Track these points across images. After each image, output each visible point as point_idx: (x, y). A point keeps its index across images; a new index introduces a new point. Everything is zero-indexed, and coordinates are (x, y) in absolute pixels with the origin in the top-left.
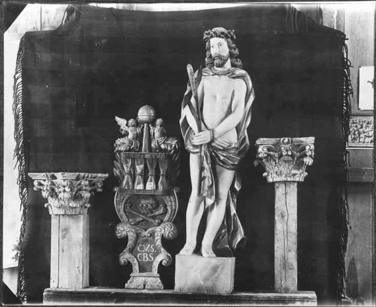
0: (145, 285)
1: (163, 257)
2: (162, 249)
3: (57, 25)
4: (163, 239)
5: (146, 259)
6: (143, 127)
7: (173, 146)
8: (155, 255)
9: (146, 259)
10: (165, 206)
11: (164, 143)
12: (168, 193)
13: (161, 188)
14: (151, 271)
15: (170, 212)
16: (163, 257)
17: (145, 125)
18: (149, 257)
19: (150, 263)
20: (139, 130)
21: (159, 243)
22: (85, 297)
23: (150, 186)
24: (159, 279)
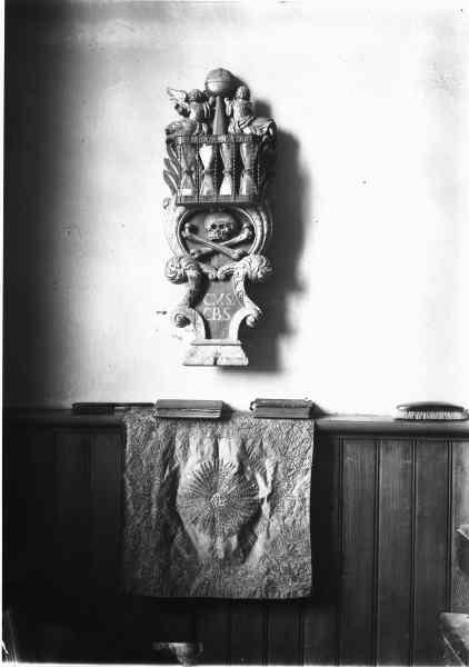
0: (216, 360)
1: (249, 310)
2: (246, 299)
3: (80, 36)
4: (248, 281)
5: (217, 317)
6: (214, 103)
7: (265, 130)
8: (233, 311)
9: (217, 317)
10: (251, 228)
11: (249, 124)
12: (255, 203)
13: (244, 191)
14: (226, 336)
15: (258, 242)
16: (249, 310)
17: (218, 98)
18: (222, 313)
19: (224, 325)
20: (206, 106)
21: (241, 287)
22: (451, 635)
23: (226, 188)
24: (239, 348)
